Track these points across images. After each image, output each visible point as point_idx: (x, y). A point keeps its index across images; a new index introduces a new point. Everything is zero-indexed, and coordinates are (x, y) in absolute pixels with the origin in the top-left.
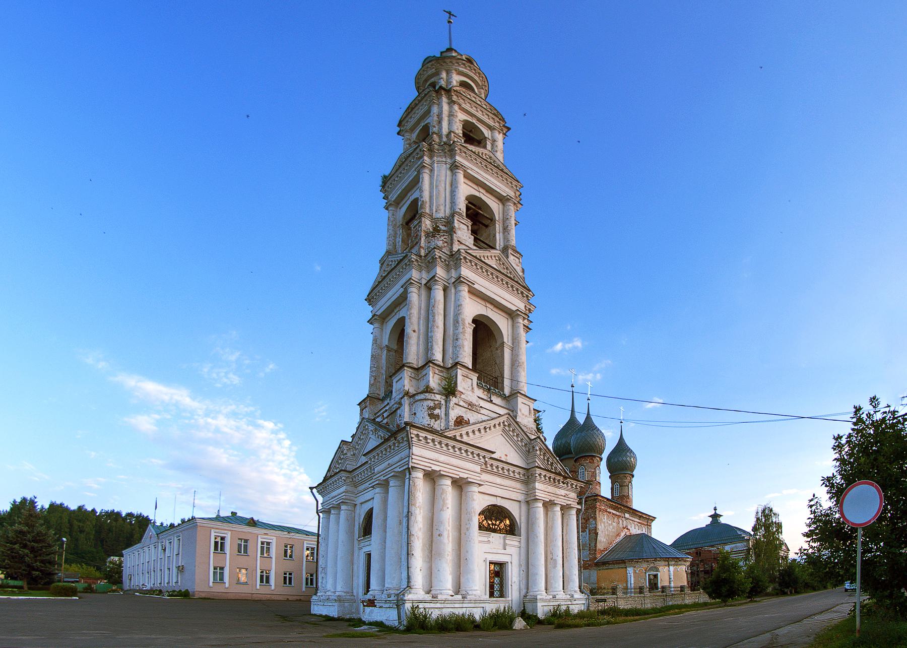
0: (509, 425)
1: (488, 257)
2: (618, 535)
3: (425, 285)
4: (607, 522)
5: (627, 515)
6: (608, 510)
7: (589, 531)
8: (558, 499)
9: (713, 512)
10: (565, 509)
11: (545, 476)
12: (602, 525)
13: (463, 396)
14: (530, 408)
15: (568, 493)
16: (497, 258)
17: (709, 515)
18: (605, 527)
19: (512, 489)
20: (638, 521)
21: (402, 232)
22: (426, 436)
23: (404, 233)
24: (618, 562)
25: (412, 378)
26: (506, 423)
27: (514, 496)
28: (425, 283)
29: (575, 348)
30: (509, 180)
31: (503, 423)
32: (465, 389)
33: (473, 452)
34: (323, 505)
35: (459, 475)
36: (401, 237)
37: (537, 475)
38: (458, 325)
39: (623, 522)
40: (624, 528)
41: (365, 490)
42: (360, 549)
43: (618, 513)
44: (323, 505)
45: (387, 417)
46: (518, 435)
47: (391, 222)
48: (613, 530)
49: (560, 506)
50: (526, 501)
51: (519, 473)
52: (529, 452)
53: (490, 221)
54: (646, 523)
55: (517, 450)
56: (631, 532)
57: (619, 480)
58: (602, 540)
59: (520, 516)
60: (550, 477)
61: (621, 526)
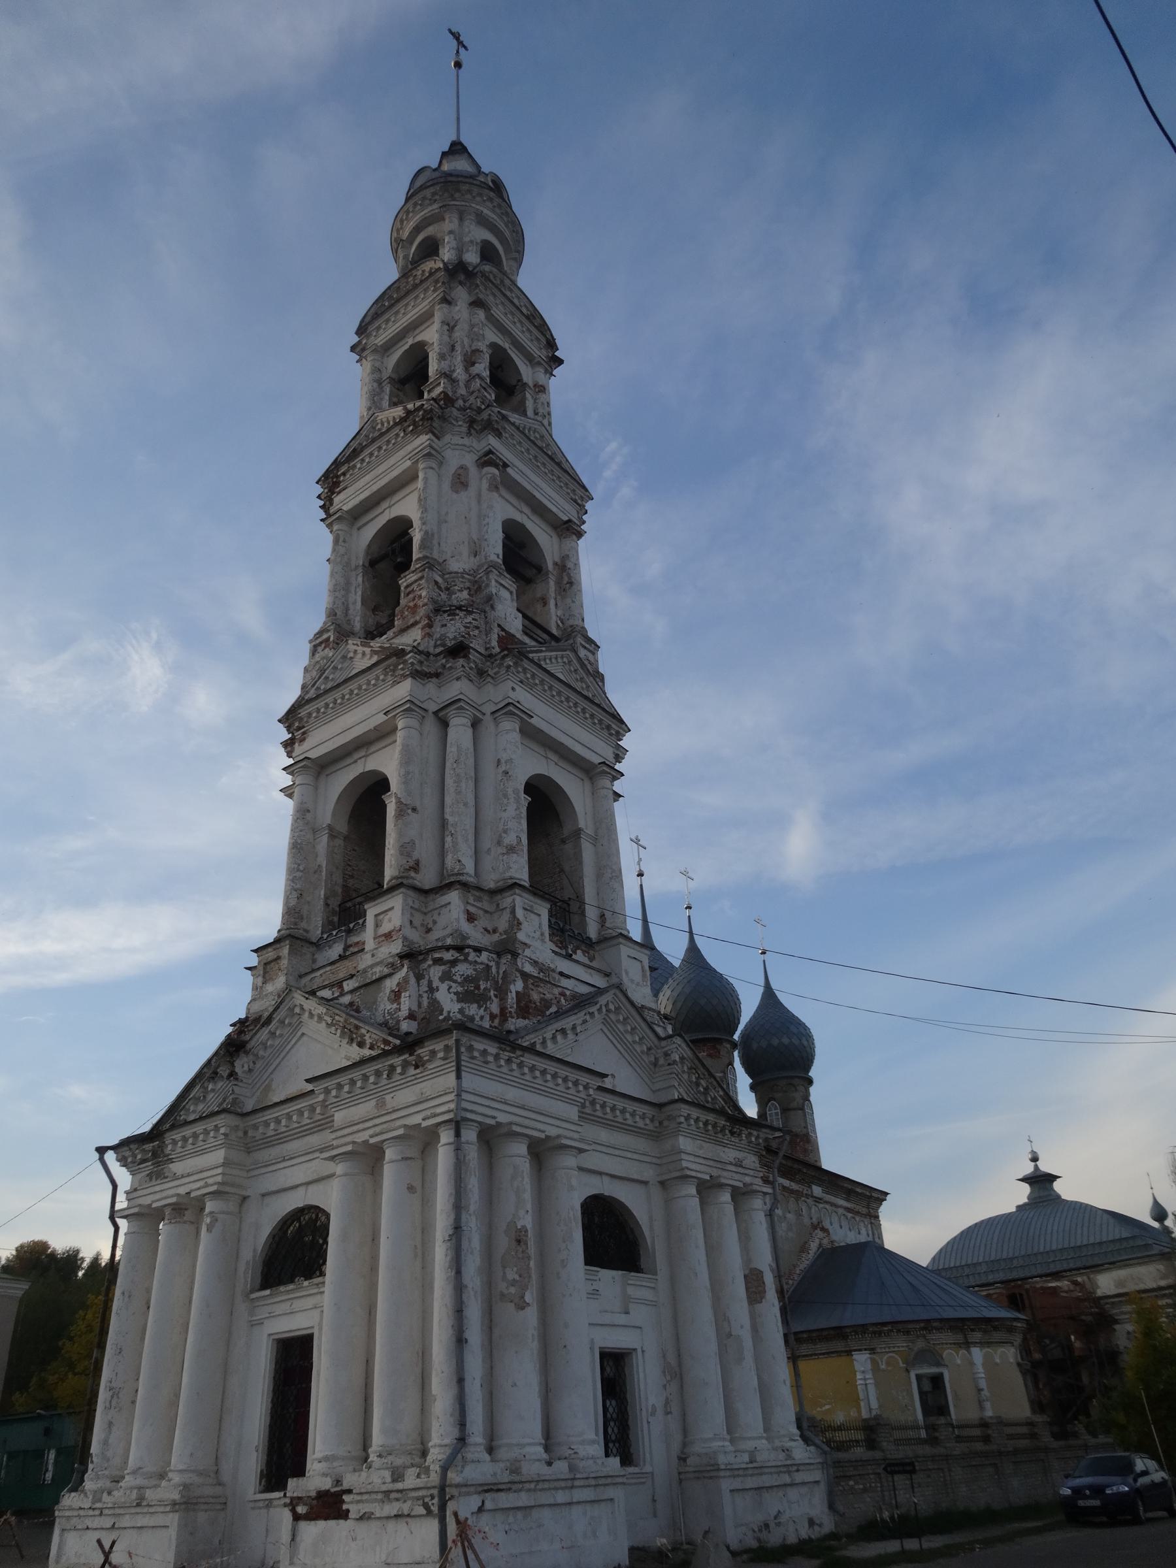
0: (618, 1009)
1: (550, 659)
2: (804, 1248)
3: (436, 713)
5: (817, 1191)
8: (725, 1174)
9: (1029, 1168)
10: (740, 1195)
11: (697, 1120)
13: (527, 952)
14: (643, 967)
15: (740, 1155)
16: (565, 660)
17: (1020, 1177)
19: (629, 1155)
21: (363, 581)
22: (486, 1047)
23: (366, 583)
24: (825, 1333)
25: (416, 909)
26: (612, 1007)
27: (633, 1171)
28: (435, 710)
29: (1076, 1338)
30: (532, 452)
31: (607, 1005)
32: (529, 936)
33: (556, 1073)
34: (132, 1195)
35: (544, 1132)
36: (359, 593)
37: (682, 1119)
38: (505, 801)
39: (810, 1208)
41: (284, 1160)
42: (254, 1324)
43: (794, 1186)
44: (132, 1195)
45: (351, 992)
46: (633, 1029)
47: (340, 559)
49: (729, 1190)
50: (659, 1182)
51: (643, 1117)
52: (655, 1064)
53: (534, 571)
54: (864, 1211)
55: (632, 1063)
56: (834, 1238)
59: (651, 1219)
60: (707, 1121)
61: (806, 1221)
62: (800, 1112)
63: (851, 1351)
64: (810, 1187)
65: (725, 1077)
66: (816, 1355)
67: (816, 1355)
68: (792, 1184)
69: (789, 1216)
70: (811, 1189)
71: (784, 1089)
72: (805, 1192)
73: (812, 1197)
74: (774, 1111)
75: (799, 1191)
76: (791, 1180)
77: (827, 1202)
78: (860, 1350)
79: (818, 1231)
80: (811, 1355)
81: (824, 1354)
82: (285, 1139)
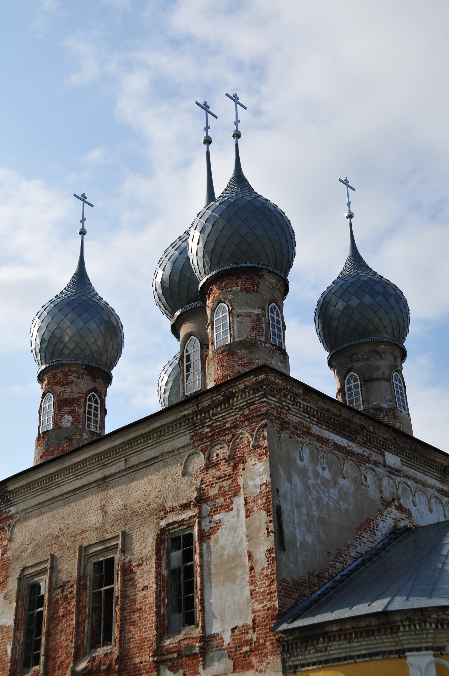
4: (316, 474)
6: (316, 430)
7: (246, 503)
12: (296, 479)
18: (307, 487)
20: (438, 484)
39: (380, 480)
40: (387, 504)
43: (354, 447)
48: (343, 505)
57: (358, 365)
58: (299, 537)
62: (386, 383)
63: (404, 651)
64: (382, 454)
65: (264, 315)
66: (352, 657)
67: (352, 657)
68: (351, 444)
69: (341, 481)
70: (384, 456)
71: (366, 357)
72: (373, 458)
73: (385, 466)
74: (352, 384)
75: (363, 456)
76: (352, 440)
77: (408, 477)
78: (419, 649)
79: (392, 509)
80: (345, 658)
81: (364, 656)
82: (16, 503)
